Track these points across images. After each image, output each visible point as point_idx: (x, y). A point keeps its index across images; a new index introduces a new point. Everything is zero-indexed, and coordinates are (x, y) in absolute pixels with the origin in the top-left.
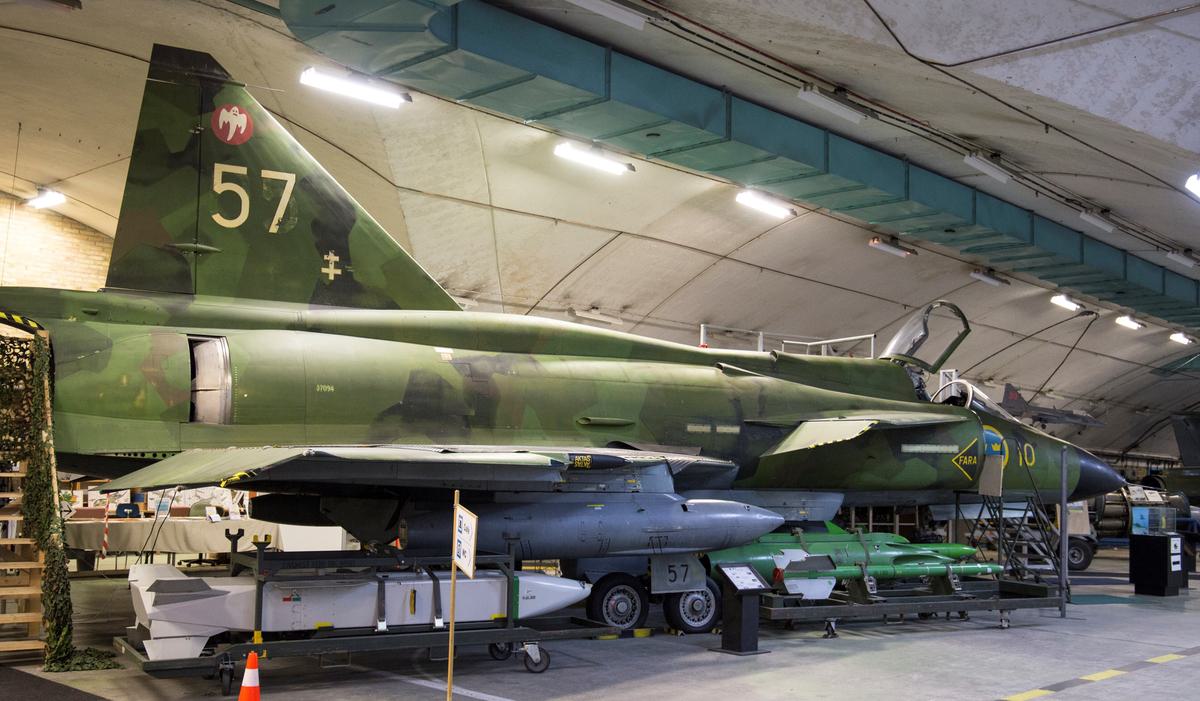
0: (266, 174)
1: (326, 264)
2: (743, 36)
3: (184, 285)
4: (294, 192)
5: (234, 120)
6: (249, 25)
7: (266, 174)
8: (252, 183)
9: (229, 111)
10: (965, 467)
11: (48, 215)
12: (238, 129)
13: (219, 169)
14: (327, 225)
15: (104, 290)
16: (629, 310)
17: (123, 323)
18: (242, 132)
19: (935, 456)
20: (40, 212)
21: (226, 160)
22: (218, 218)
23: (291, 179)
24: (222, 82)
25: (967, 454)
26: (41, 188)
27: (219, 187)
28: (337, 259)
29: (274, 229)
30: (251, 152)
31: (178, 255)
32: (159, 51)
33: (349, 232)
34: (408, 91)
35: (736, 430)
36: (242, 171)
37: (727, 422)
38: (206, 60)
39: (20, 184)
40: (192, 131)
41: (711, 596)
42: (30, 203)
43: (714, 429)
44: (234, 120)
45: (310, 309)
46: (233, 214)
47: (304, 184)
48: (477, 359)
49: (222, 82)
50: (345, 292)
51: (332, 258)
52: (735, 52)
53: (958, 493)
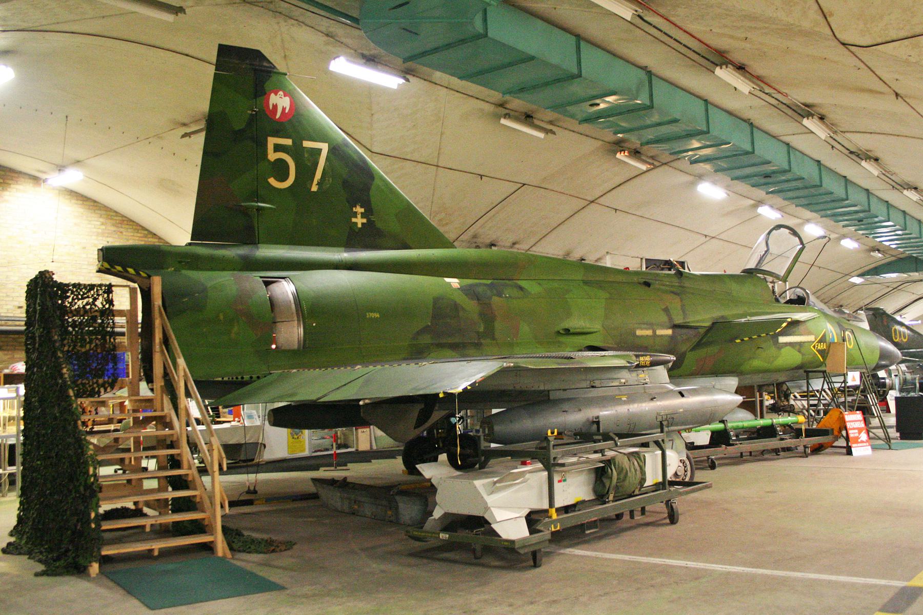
0: (307, 144)
1: (355, 215)
2: (690, 27)
3: (250, 238)
4: (327, 159)
5: (280, 102)
6: (293, 25)
7: (307, 144)
8: (296, 151)
9: (276, 94)
10: (819, 351)
11: (60, 190)
12: (284, 109)
13: (272, 141)
14: (354, 181)
15: (190, 244)
16: (517, 246)
17: (208, 270)
18: (287, 111)
19: (800, 344)
20: (54, 189)
21: (276, 134)
22: (272, 181)
23: (324, 147)
24: (270, 72)
25: (820, 341)
26: (61, 168)
27: (272, 156)
28: (363, 210)
29: (314, 188)
30: (294, 125)
31: (245, 212)
32: (224, 50)
33: (369, 189)
34: (406, 73)
35: (669, 332)
36: (288, 142)
37: (663, 327)
38: (257, 55)
39: (41, 166)
40: (249, 112)
41: (688, 463)
42: (49, 182)
43: (654, 332)
44: (280, 102)
45: (345, 251)
46: (283, 177)
47: (335, 150)
48: (476, 285)
49: (270, 72)
50: (370, 237)
51: (359, 210)
52: (675, 40)
53: (807, 372)
